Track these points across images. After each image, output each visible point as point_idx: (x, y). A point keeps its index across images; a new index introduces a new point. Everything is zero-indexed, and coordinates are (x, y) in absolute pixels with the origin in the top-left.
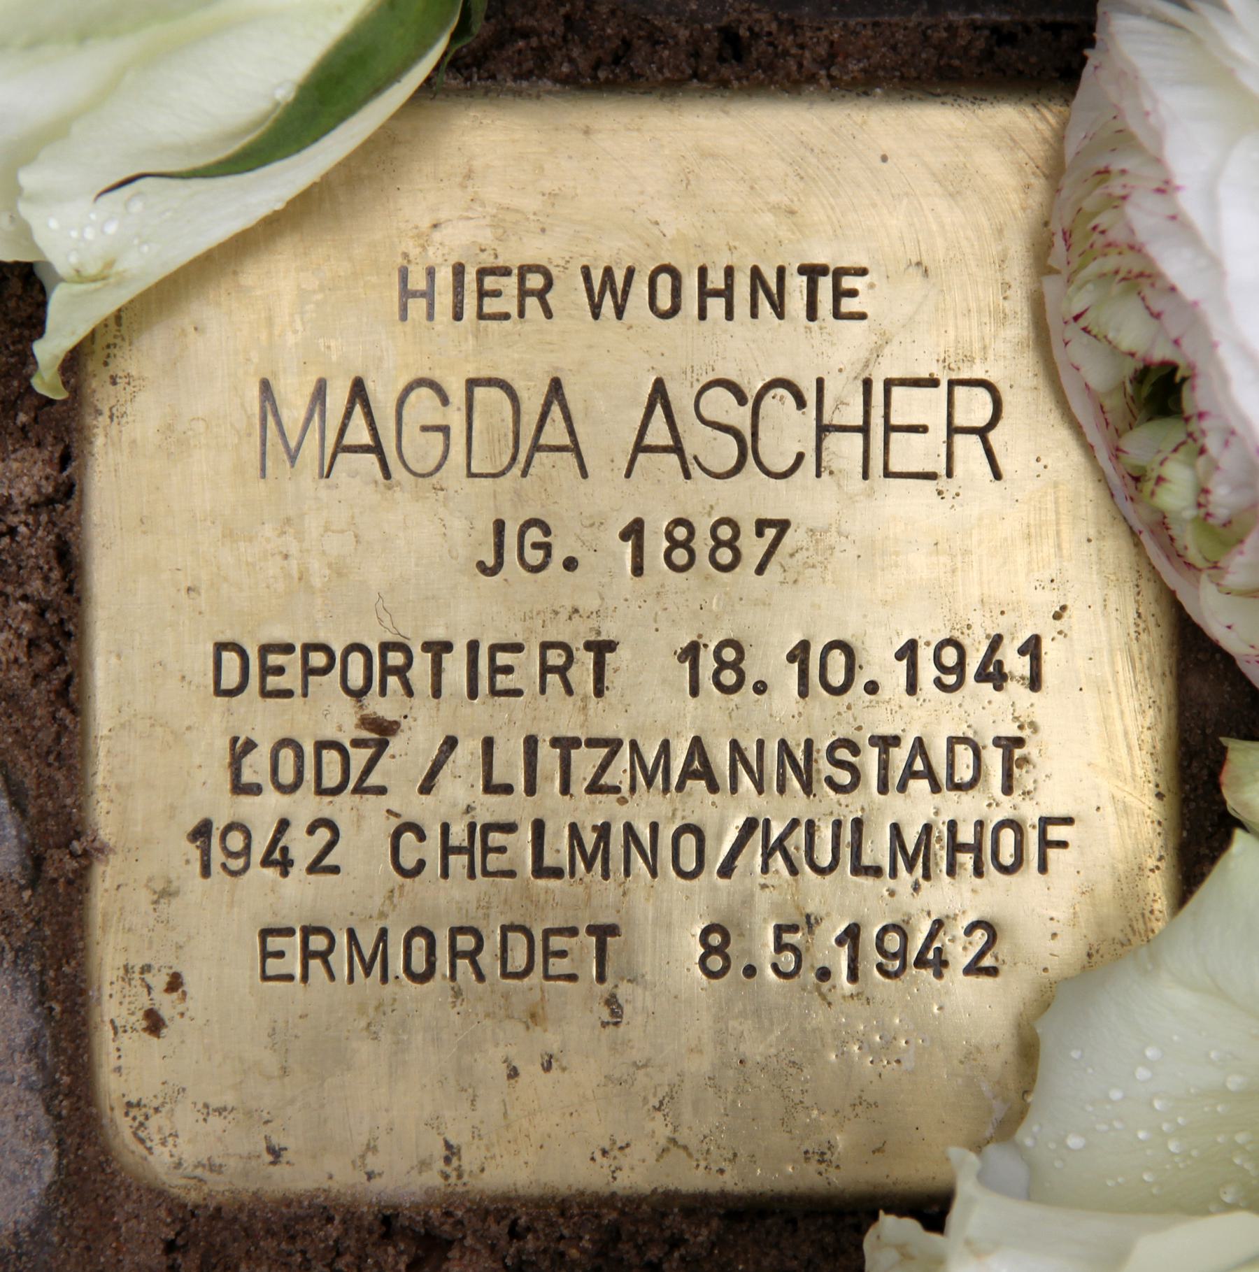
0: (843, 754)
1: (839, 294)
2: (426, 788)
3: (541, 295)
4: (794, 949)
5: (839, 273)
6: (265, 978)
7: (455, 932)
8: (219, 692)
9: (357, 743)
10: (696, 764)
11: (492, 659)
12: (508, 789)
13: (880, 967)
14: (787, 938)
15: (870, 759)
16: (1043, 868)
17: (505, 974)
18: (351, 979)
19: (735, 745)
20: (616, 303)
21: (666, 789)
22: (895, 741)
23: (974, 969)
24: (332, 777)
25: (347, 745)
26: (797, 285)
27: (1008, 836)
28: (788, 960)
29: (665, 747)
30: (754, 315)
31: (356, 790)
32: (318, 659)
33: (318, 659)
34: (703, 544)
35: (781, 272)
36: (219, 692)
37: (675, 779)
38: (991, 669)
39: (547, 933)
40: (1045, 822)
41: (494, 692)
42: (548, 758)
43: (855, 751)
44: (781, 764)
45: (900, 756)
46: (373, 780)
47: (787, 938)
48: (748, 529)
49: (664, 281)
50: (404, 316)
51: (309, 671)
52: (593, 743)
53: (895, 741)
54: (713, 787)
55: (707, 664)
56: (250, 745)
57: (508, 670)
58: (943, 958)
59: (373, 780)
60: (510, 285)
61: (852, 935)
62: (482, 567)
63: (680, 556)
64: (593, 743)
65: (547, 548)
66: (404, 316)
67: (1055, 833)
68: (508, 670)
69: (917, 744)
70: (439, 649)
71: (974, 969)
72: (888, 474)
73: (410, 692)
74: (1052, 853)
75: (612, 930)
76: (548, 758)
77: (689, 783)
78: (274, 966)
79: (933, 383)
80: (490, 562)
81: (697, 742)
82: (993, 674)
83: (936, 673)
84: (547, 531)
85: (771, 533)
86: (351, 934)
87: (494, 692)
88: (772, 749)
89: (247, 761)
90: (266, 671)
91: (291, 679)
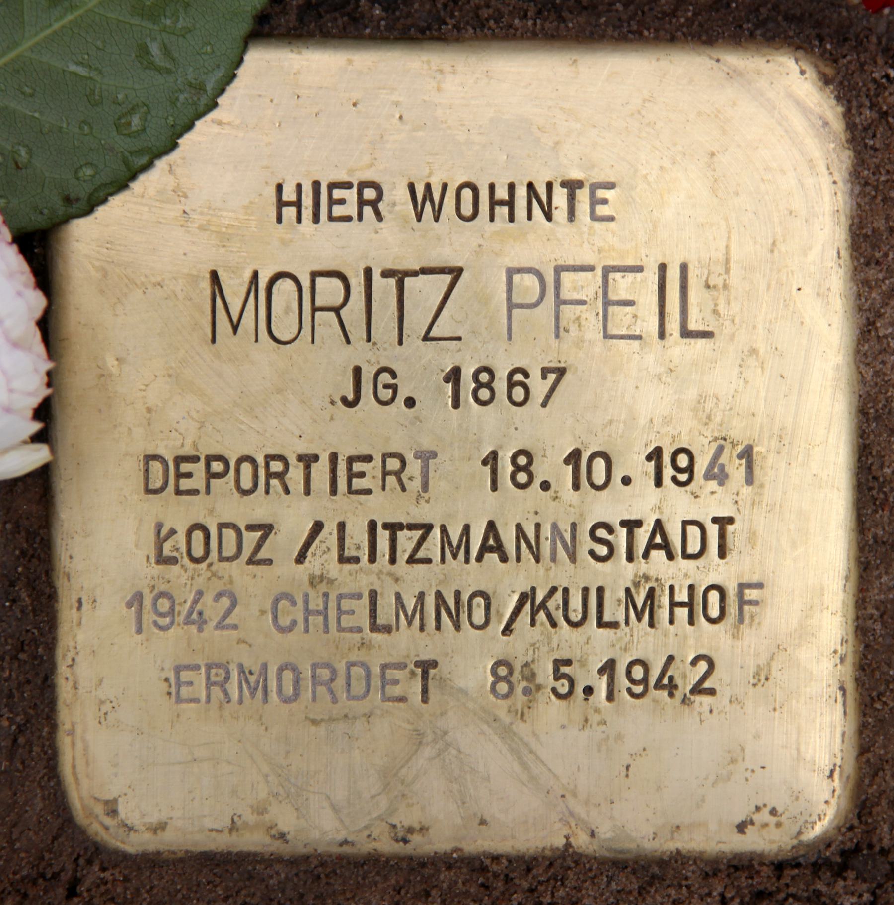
0: (602, 533)
1: (595, 202)
3: (374, 204)
4: (565, 676)
5: (594, 187)
8: (148, 491)
9: (251, 528)
10: (491, 542)
11: (349, 469)
13: (629, 691)
14: (565, 669)
18: (241, 702)
19: (519, 527)
21: (467, 561)
22: (639, 523)
25: (243, 529)
26: (560, 198)
27: (714, 596)
29: (467, 529)
30: (530, 217)
31: (251, 562)
32: (217, 467)
33: (217, 467)
34: (501, 386)
35: (550, 185)
36: (148, 491)
37: (474, 552)
38: (716, 470)
40: (742, 587)
41: (350, 491)
42: (383, 537)
43: (610, 530)
44: (554, 543)
45: (642, 536)
46: (262, 555)
47: (565, 669)
48: (536, 373)
49: (467, 194)
50: (279, 220)
51: (211, 476)
52: (411, 527)
53: (639, 523)
54: (504, 559)
57: (362, 475)
58: (674, 683)
59: (261, 555)
60: (351, 195)
61: (609, 668)
62: (344, 400)
63: (484, 394)
64: (411, 527)
65: (395, 388)
66: (279, 220)
68: (362, 475)
69: (465, 532)
72: (686, 333)
76: (383, 537)
77: (487, 556)
79: (591, 268)
80: (351, 397)
82: (717, 474)
84: (394, 375)
85: (552, 377)
87: (350, 491)
90: (179, 476)
91: (198, 481)
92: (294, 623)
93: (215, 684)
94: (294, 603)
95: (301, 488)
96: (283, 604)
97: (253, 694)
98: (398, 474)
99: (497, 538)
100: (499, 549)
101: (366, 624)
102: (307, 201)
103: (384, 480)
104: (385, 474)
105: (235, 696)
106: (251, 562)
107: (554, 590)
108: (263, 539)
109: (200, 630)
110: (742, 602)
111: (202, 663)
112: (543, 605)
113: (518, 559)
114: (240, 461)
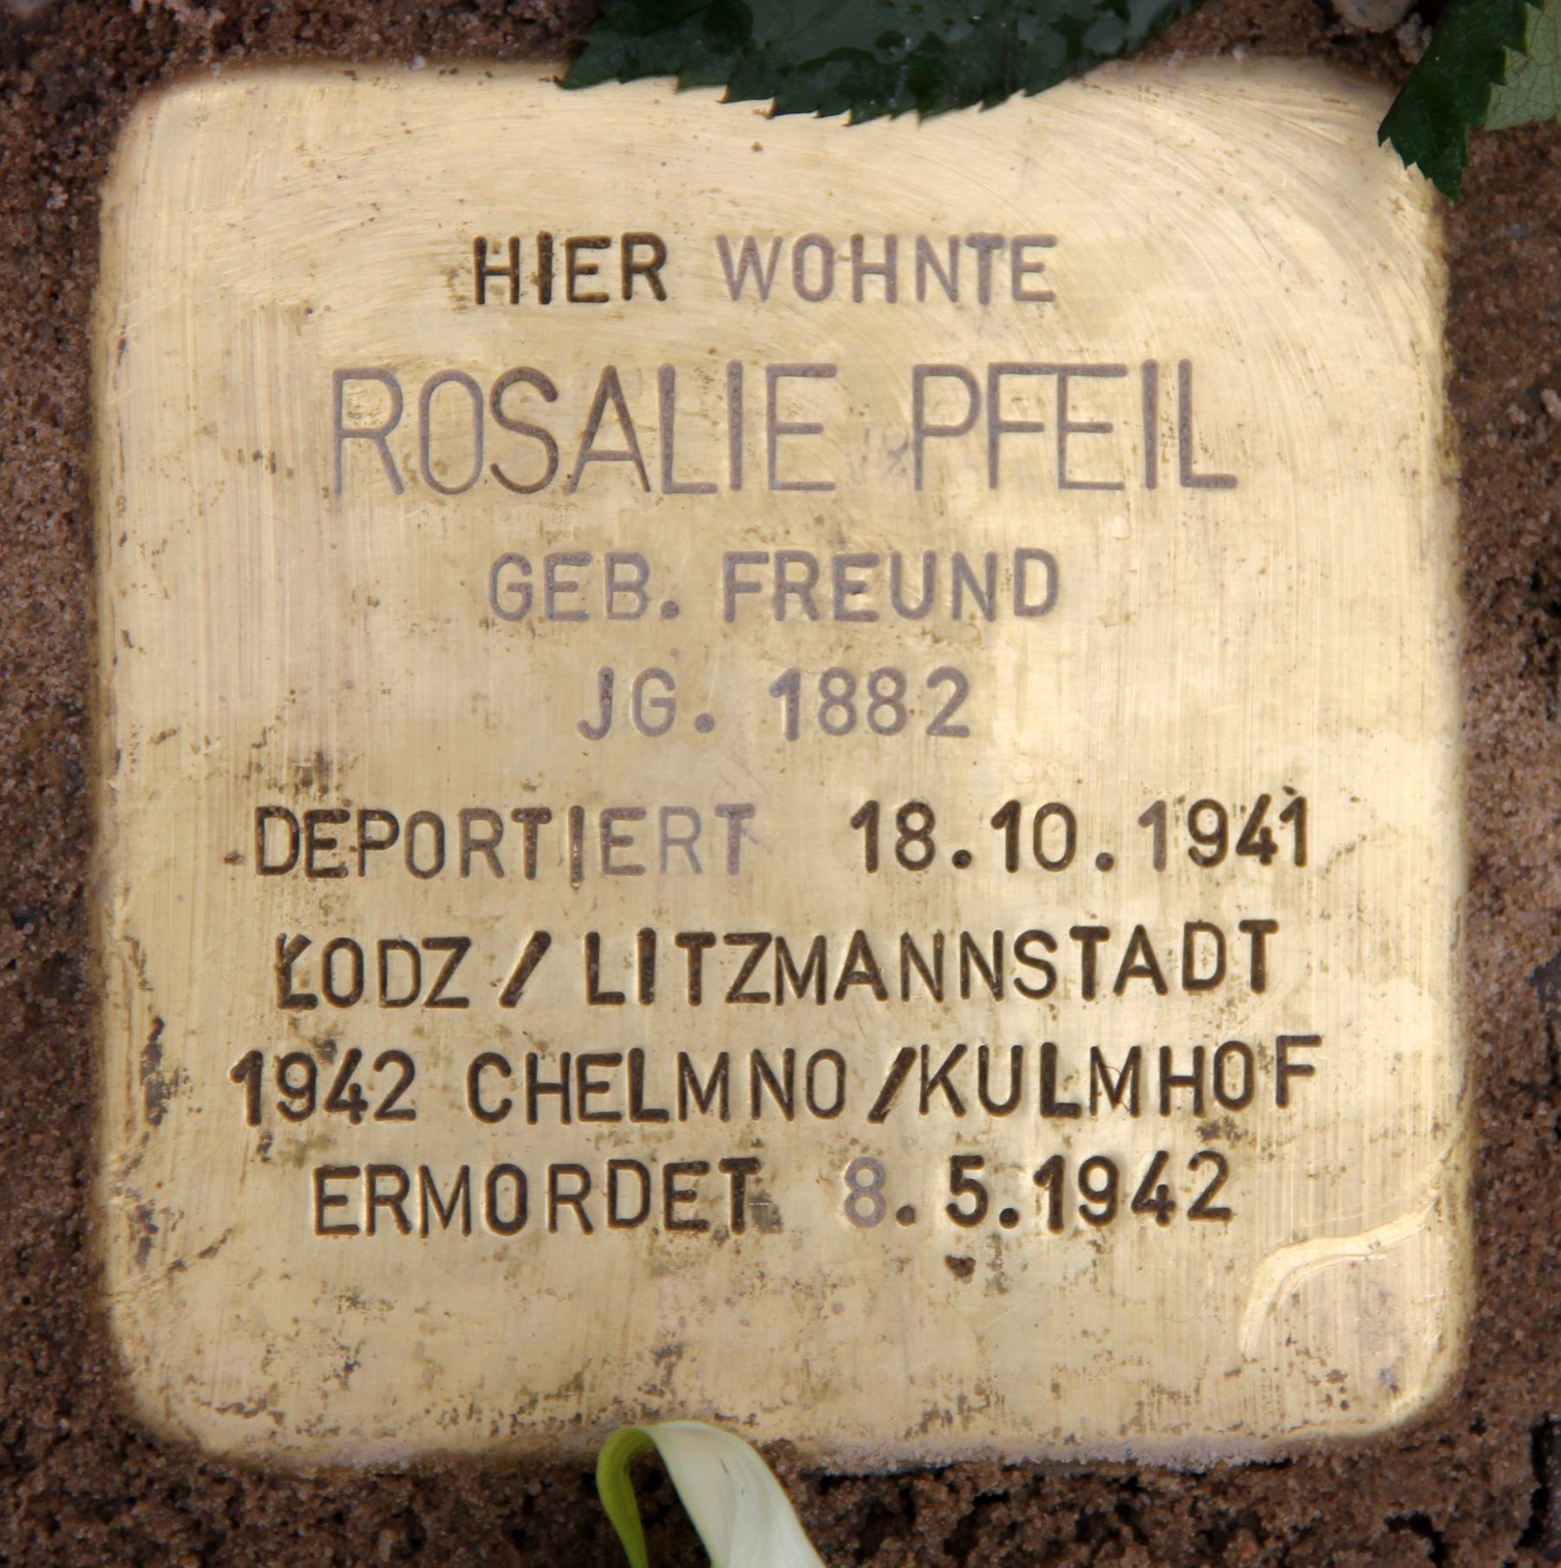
0: (1034, 949)
1: (1019, 270)
2: (510, 999)
4: (974, 1186)
5: (1019, 244)
6: (322, 1229)
7: (555, 1170)
8: (266, 870)
9: (430, 943)
12: (618, 998)
15: (1069, 957)
16: (1283, 1099)
17: (615, 1221)
18: (425, 1230)
19: (906, 940)
20: (760, 281)
21: (821, 998)
22: (1103, 933)
23: (1200, 1210)
24: (401, 984)
28: (968, 1202)
29: (820, 945)
31: (432, 1002)
33: (378, 830)
39: (672, 1170)
43: (1051, 944)
45: (1111, 956)
46: (451, 990)
49: (814, 256)
51: (366, 845)
53: (1103, 933)
54: (882, 994)
55: (889, 834)
56: (302, 943)
59: (450, 991)
67: (1297, 1056)
70: (535, 817)
71: (1200, 1210)
73: (499, 870)
74: (1294, 1082)
75: (752, 1165)
78: (333, 1215)
81: (860, 936)
83: (1191, 842)
86: (425, 1172)
88: (953, 946)
89: (300, 962)
91: (343, 855)
92: (507, 1105)
93: (567, 1199)
94: (506, 1070)
95: (521, 867)
96: (490, 1074)
97: (446, 1219)
98: (688, 843)
99: (1149, 955)
100: (874, 977)
101: (625, 1107)
102: (530, 264)
103: (664, 855)
104: (667, 841)
105: (416, 1221)
106: (432, 1002)
107: (960, 1050)
108: (456, 959)
109: (356, 1119)
110: (1285, 1071)
111: (363, 1167)
112: (942, 1076)
113: (906, 995)
114: (413, 823)
